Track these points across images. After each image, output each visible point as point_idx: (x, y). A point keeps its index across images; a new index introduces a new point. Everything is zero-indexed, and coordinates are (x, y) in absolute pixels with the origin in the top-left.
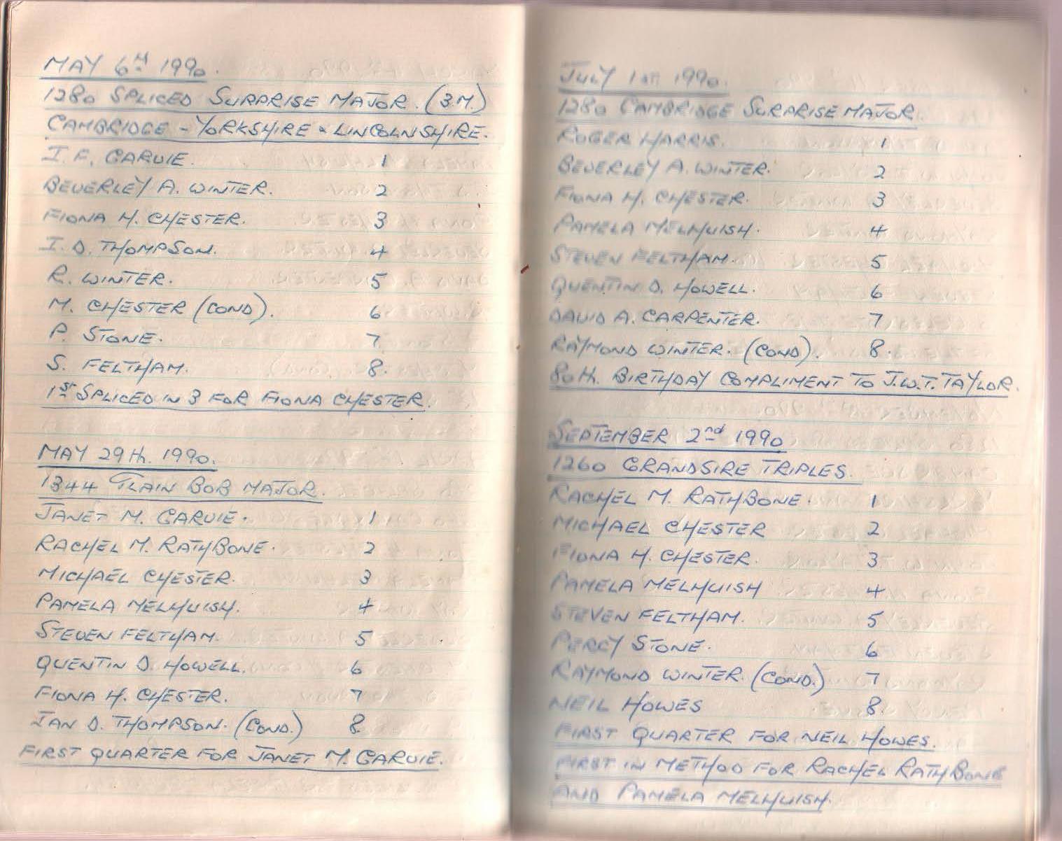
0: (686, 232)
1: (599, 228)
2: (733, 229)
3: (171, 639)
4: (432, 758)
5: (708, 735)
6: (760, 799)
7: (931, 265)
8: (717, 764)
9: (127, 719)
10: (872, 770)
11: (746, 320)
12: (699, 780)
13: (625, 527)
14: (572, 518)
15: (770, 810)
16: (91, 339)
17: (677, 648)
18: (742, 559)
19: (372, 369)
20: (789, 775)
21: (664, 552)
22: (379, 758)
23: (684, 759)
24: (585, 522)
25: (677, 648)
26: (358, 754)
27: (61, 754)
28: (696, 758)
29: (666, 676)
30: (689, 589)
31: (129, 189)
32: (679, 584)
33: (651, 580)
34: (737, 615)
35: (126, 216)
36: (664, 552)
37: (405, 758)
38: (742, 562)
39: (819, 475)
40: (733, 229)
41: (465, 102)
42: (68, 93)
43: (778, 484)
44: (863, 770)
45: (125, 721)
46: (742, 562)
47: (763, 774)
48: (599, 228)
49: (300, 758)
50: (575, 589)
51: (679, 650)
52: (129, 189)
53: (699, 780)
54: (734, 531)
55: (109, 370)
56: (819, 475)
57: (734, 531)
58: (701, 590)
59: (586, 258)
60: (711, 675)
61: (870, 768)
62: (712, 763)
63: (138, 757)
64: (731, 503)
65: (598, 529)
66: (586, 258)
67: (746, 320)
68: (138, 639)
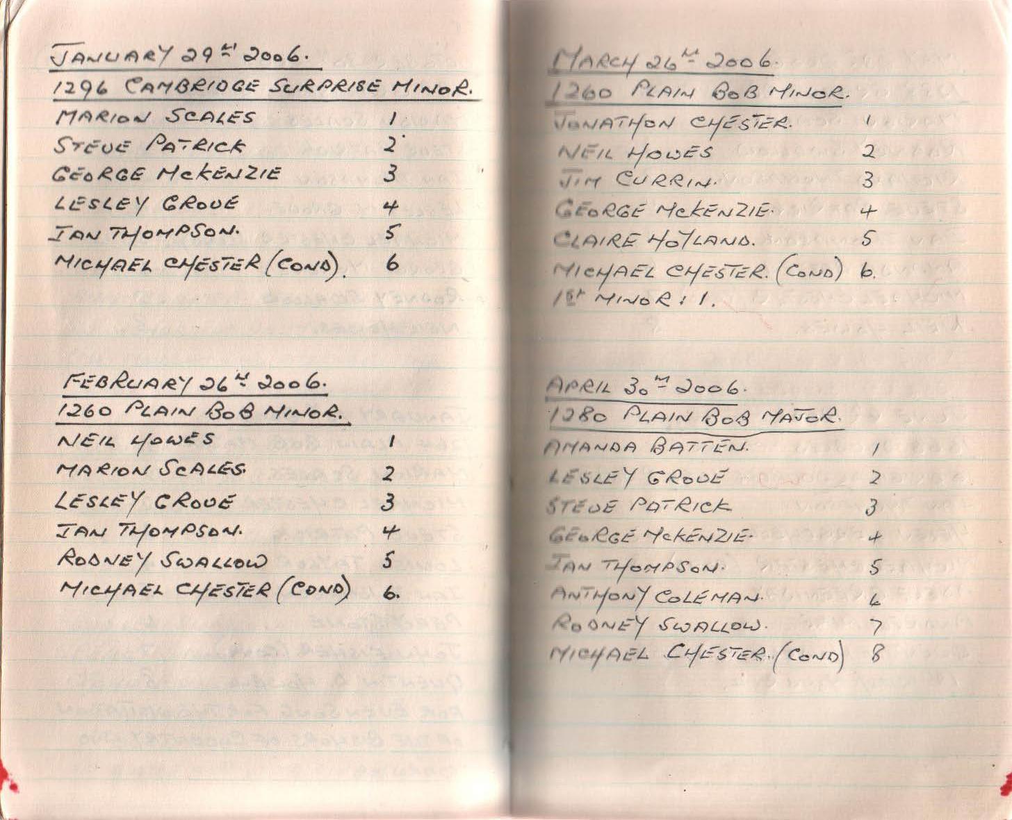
2: (217, 264)
3: (616, 568)
4: (88, 381)
6: (621, 61)
7: (951, 448)
8: (630, 566)
10: (252, 590)
11: (261, 591)
12: (656, 239)
13: (138, 591)
15: (629, 73)
22: (658, 416)
23: (587, 535)
24: (591, 270)
26: (276, 597)
27: (92, 206)
28: (692, 442)
29: (176, 112)
30: (650, 419)
31: (254, 86)
35: (713, 123)
37: (196, 204)
38: (662, 303)
40: (217, 264)
41: (165, 88)
44: (196, 264)
46: (662, 303)
49: (239, 117)
52: (254, 86)
53: (656, 239)
54: (711, 447)
57: (711, 447)
60: (737, 655)
61: (203, 261)
63: (102, 178)
65: (713, 128)
67: (261, 591)
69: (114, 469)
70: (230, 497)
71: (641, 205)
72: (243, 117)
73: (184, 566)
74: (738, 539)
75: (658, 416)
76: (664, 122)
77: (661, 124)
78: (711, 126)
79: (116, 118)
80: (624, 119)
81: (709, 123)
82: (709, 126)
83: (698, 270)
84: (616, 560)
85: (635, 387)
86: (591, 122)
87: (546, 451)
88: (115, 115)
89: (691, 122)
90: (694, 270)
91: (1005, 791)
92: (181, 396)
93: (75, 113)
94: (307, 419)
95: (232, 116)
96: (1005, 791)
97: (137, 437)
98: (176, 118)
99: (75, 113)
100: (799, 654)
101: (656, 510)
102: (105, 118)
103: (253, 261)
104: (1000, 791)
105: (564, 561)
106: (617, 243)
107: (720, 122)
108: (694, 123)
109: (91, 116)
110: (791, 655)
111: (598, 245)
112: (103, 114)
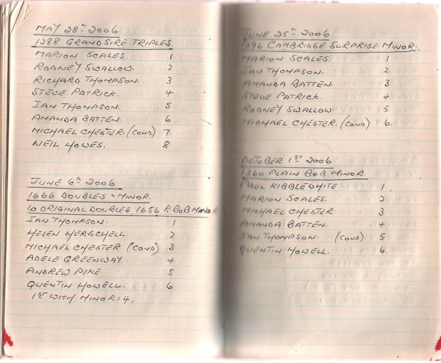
0: (130, 81)
1: (321, 111)
5: (322, 212)
9: (91, 78)
14: (250, 209)
16: (307, 32)
17: (326, 85)
18: (329, 212)
19: (165, 145)
20: (297, 46)
21: (185, 210)
22: (62, 80)
25: (326, 85)
32: (47, 259)
33: (83, 296)
34: (47, 118)
36: (185, 210)
39: (300, 188)
42: (53, 41)
43: (278, 111)
45: (272, 249)
47: (298, 43)
48: (321, 111)
50: (251, 239)
51: (327, 86)
55: (70, 133)
56: (300, 188)
58: (42, 29)
59: (248, 250)
62: (273, 236)
64: (269, 239)
65: (299, 213)
66: (248, 250)
68: (275, 214)
69: (267, 225)
70: (321, 57)
71: (307, 210)
72: (320, 199)
73: (305, 253)
74: (318, 60)
75: (62, 80)
76: (37, 272)
77: (36, 272)
78: (90, 133)
79: (269, 59)
80: (43, 91)
81: (88, 132)
82: (88, 133)
83: (93, 131)
84: (273, 68)
85: (324, 174)
86: (269, 84)
87: (241, 225)
88: (267, 198)
89: (178, 205)
90: (304, 123)
91: (438, 348)
92: (30, 221)
93: (43, 53)
94: (350, 177)
95: (48, 233)
96: (438, 348)
97: (274, 183)
98: (291, 199)
99: (43, 53)
100: (136, 132)
101: (83, 94)
102: (362, 46)
103: (273, 185)
104: (435, 347)
105: (249, 70)
106: (40, 81)
107: (107, 234)
108: (291, 212)
109: (264, 84)
110: (43, 64)
111: (66, 82)
112: (38, 78)
